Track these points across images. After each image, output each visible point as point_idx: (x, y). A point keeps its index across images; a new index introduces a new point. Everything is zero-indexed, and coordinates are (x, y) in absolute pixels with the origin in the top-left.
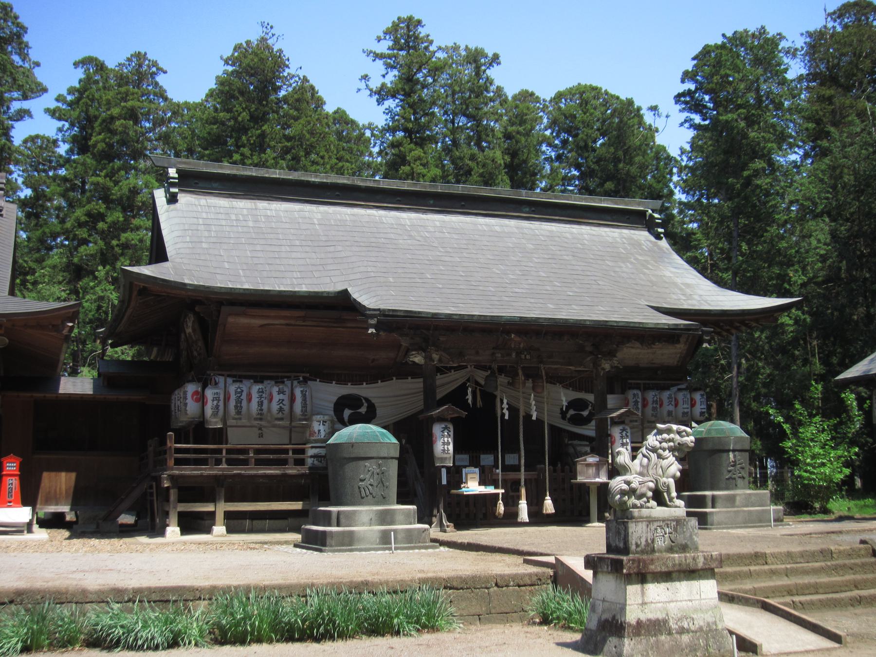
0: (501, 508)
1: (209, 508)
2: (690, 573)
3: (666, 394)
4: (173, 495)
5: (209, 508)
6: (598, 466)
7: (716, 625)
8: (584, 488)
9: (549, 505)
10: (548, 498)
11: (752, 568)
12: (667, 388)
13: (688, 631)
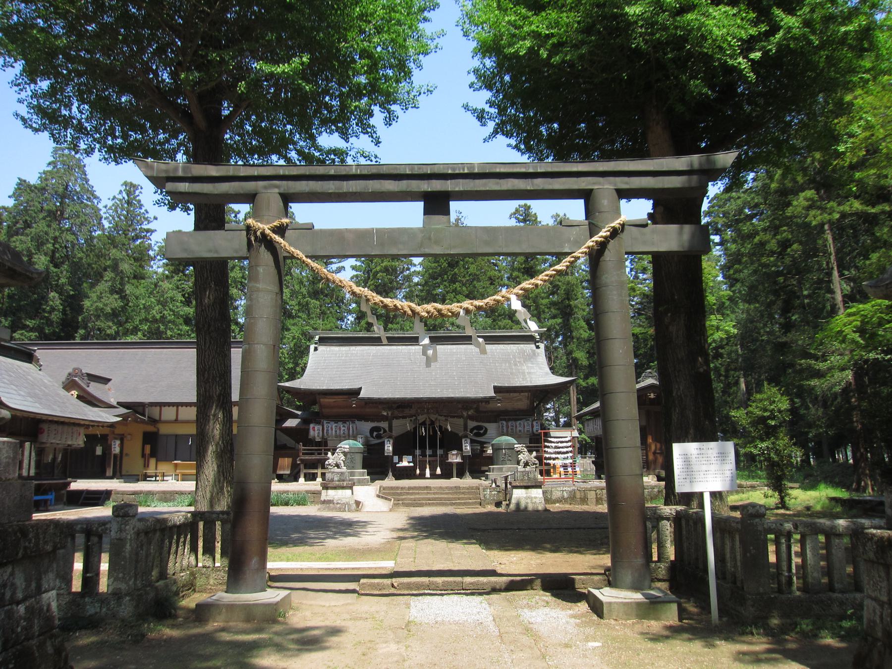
0: (418, 472)
1: (315, 471)
2: (343, 488)
3: (518, 422)
4: (302, 466)
5: (315, 471)
6: (457, 455)
8: (451, 464)
9: (439, 471)
12: (520, 419)
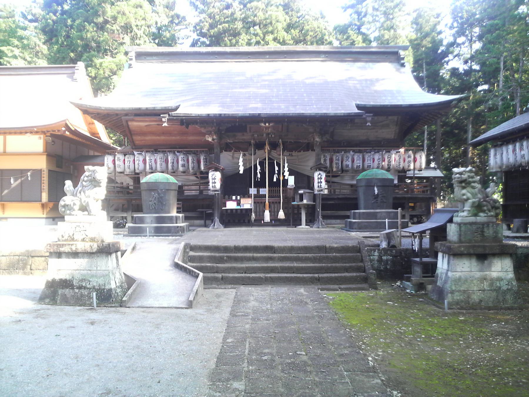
7: (105, 286)
9: (281, 215)
10: (281, 210)
11: (255, 255)
13: (85, 288)
